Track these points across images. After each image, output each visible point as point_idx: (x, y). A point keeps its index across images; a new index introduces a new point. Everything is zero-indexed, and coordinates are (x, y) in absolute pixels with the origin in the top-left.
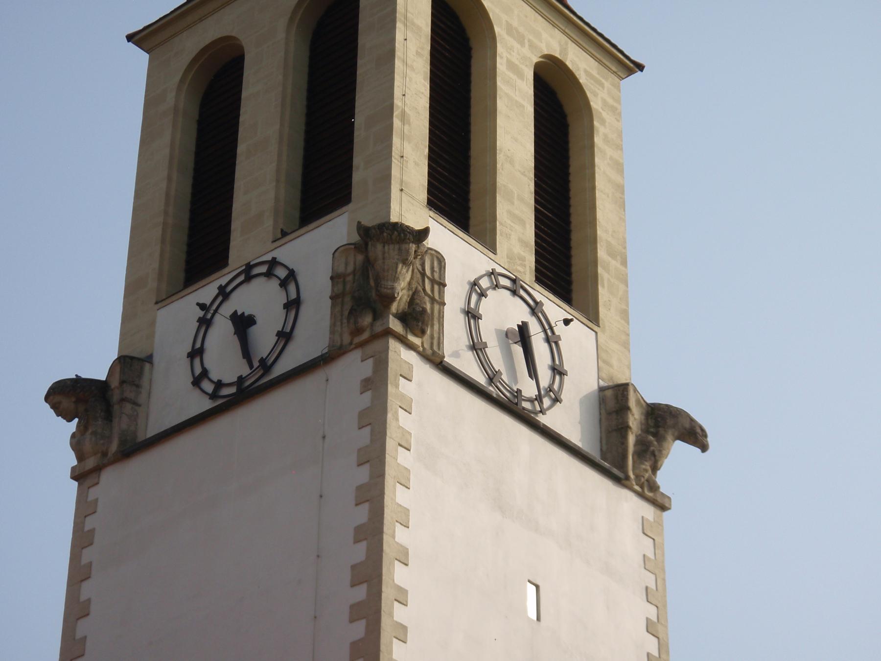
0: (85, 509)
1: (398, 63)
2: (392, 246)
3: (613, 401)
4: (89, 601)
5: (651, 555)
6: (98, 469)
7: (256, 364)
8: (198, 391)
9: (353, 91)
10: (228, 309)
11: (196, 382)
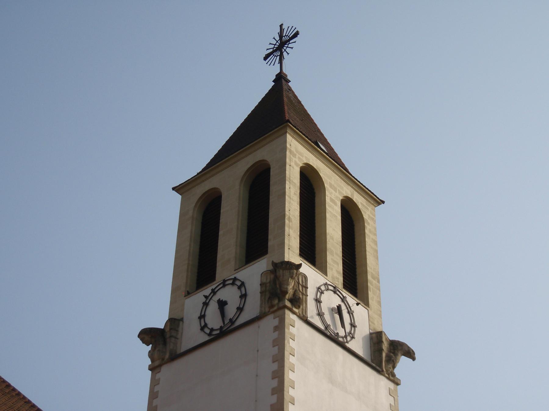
0: (154, 383)
1: (287, 197)
3: (376, 339)
5: (393, 404)
6: (160, 366)
7: (227, 321)
10: (216, 298)
11: (202, 329)
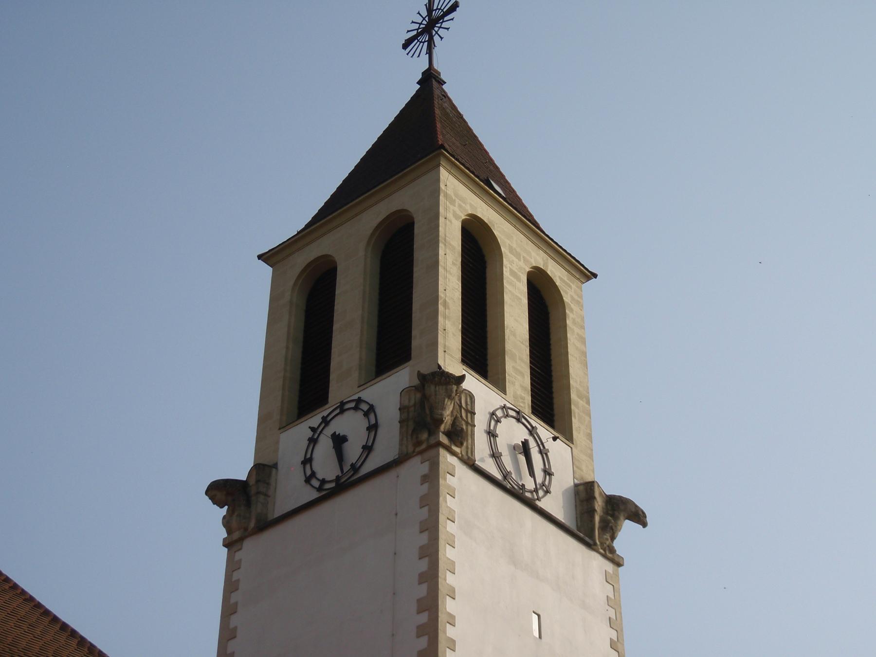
0: (232, 566)
1: (441, 270)
2: (441, 387)
3: (584, 493)
4: (236, 628)
5: (612, 596)
6: (241, 539)
7: (347, 468)
8: (308, 487)
9: (412, 287)
10: (329, 431)
11: (308, 480)
